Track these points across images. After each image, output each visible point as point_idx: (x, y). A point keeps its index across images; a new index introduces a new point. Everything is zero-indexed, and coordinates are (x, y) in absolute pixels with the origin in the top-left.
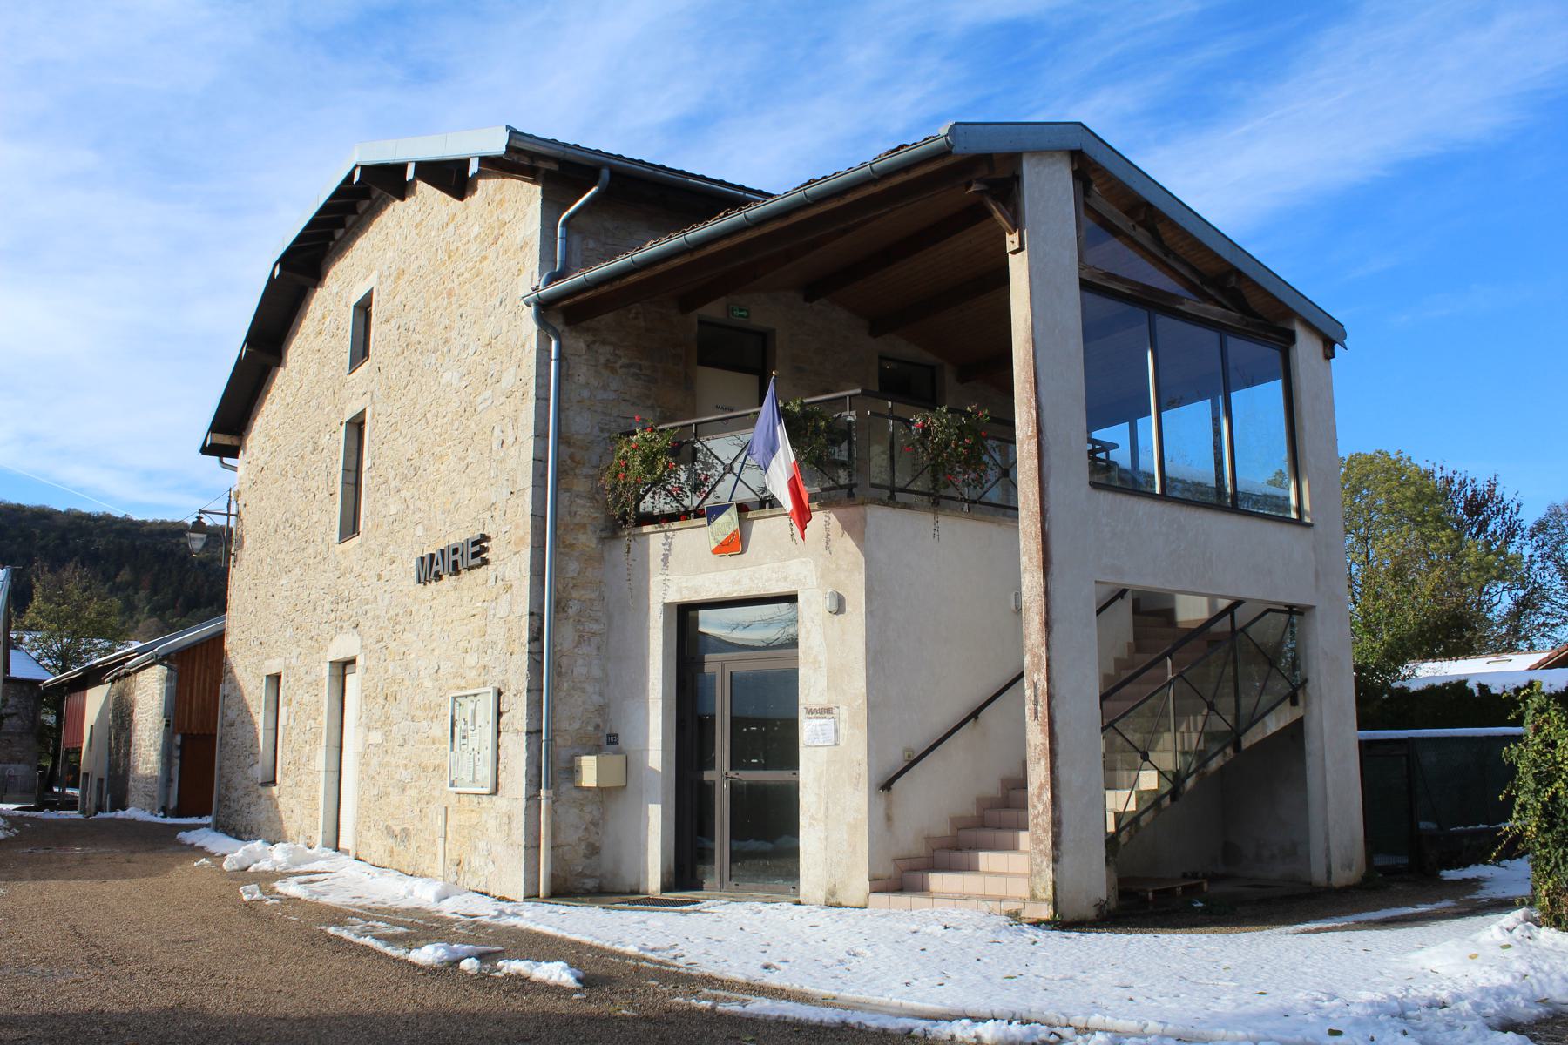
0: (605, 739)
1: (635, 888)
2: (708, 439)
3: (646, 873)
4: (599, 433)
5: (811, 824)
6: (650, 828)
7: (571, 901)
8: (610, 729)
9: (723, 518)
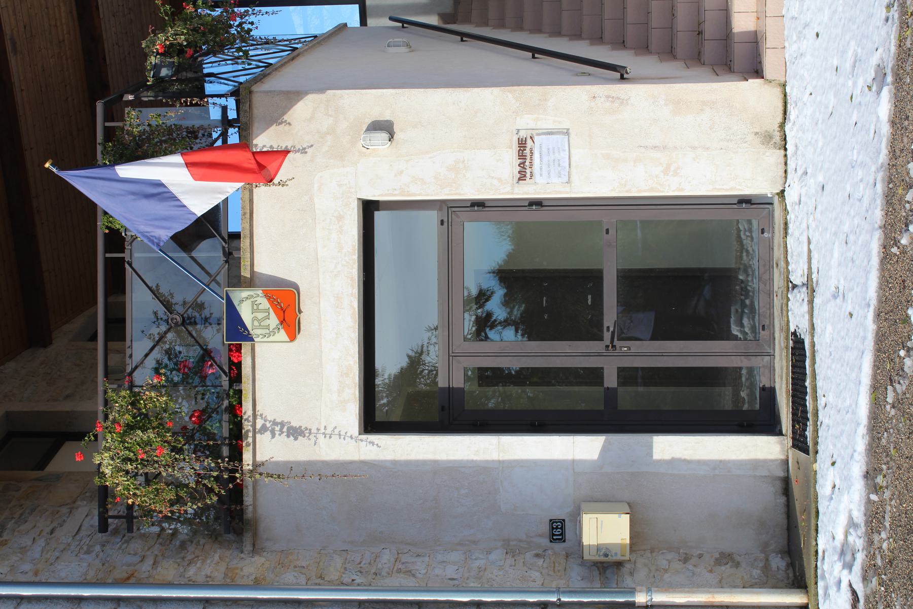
0: (558, 546)
1: (779, 485)
2: (131, 356)
3: (756, 464)
4: (93, 554)
5: (676, 173)
6: (688, 458)
7: (809, 563)
8: (540, 536)
9: (246, 313)
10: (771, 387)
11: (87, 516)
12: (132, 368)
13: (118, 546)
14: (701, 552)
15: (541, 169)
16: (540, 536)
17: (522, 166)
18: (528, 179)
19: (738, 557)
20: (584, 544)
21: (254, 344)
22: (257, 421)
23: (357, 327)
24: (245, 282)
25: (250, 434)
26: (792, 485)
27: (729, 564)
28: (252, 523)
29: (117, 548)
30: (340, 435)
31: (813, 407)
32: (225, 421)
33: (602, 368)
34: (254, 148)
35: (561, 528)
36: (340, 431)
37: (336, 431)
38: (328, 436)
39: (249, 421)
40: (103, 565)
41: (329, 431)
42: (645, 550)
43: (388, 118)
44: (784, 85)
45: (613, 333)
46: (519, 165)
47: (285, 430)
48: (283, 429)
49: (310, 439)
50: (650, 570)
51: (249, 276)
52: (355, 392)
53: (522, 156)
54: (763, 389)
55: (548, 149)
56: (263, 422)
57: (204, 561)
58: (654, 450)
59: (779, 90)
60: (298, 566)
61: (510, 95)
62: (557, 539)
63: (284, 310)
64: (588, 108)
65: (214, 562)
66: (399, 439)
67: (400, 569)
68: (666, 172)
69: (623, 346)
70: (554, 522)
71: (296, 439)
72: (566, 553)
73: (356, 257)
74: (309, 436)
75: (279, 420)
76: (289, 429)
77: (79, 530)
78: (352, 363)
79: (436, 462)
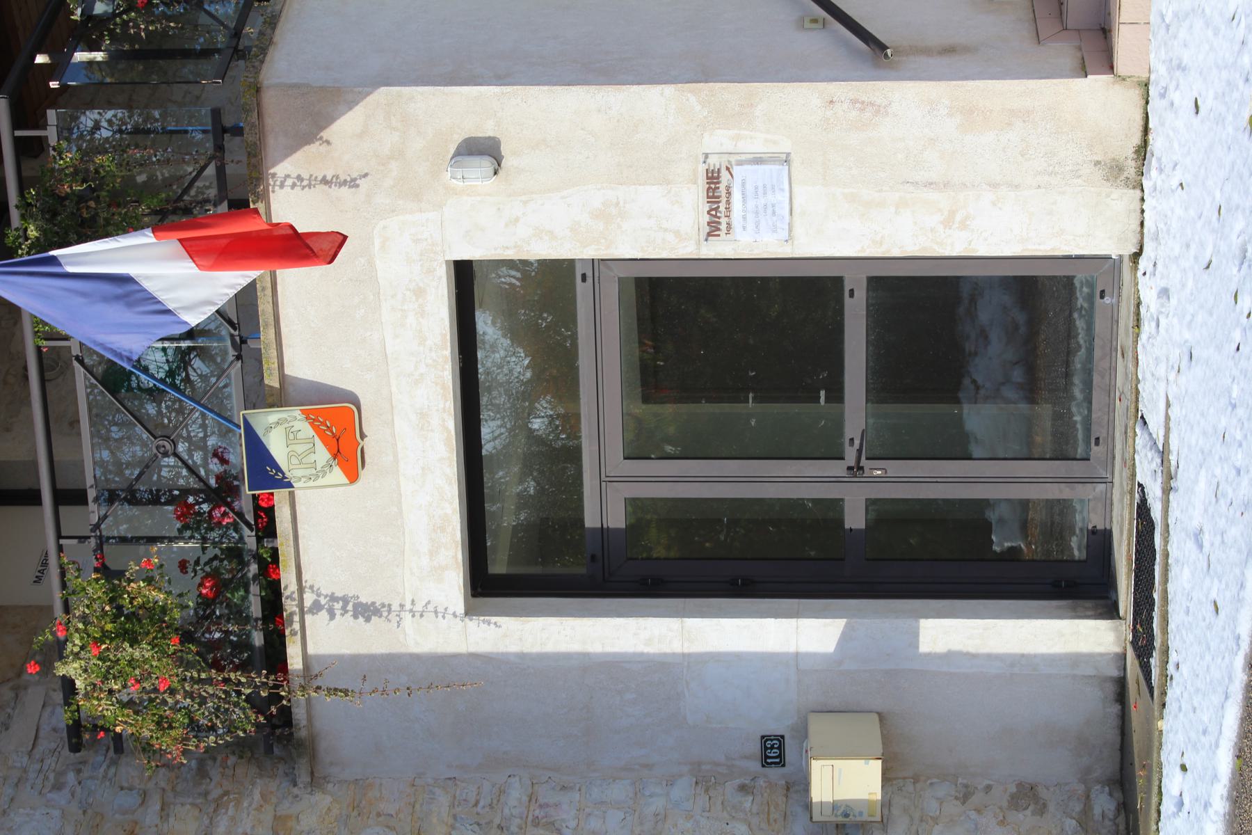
0: (774, 773)
1: (1111, 689)
3: (1076, 660)
4: (66, 792)
5: (964, 226)
6: (972, 650)
8: (746, 757)
9: (277, 446)
10: (1105, 528)
11: (44, 706)
12: (99, 517)
13: (102, 770)
14: (991, 783)
15: (744, 218)
16: (746, 757)
17: (713, 213)
18: (722, 233)
19: (1045, 791)
20: (813, 801)
21: (293, 492)
22: (305, 596)
23: (455, 459)
24: (273, 395)
25: (296, 618)
26: (1129, 693)
27: (1031, 808)
28: (308, 743)
29: (101, 776)
30: (436, 612)
31: (1162, 642)
32: (254, 595)
33: (842, 500)
34: (271, 180)
35: (779, 748)
36: (436, 607)
37: (431, 608)
38: (417, 615)
39: (293, 600)
40: (85, 812)
41: (419, 608)
42: (904, 778)
43: (490, 134)
44: (1147, 85)
45: (860, 451)
46: (709, 213)
47: (350, 607)
48: (346, 607)
49: (389, 621)
50: (912, 818)
51: (277, 385)
52: (456, 555)
53: (713, 197)
54: (1094, 532)
55: (756, 188)
56: (315, 597)
57: (238, 803)
58: (921, 639)
59: (1137, 92)
60: (384, 814)
61: (693, 99)
62: (772, 763)
63: (337, 437)
64: (821, 120)
65: (254, 806)
66: (529, 621)
67: (537, 817)
68: (947, 223)
69: (876, 470)
70: (767, 740)
71: (368, 620)
72: (786, 782)
73: (447, 352)
74: (388, 616)
75: (339, 594)
76: (356, 606)
77: (36, 737)
78: (449, 511)
79: (585, 655)
